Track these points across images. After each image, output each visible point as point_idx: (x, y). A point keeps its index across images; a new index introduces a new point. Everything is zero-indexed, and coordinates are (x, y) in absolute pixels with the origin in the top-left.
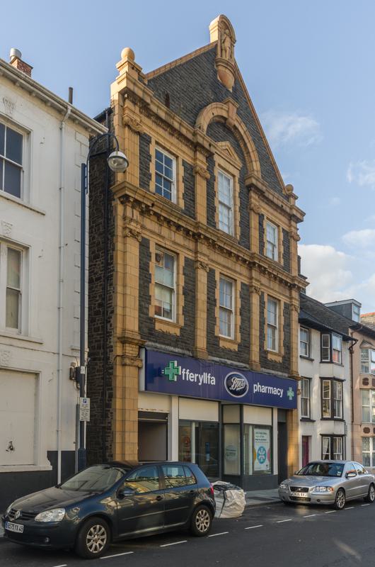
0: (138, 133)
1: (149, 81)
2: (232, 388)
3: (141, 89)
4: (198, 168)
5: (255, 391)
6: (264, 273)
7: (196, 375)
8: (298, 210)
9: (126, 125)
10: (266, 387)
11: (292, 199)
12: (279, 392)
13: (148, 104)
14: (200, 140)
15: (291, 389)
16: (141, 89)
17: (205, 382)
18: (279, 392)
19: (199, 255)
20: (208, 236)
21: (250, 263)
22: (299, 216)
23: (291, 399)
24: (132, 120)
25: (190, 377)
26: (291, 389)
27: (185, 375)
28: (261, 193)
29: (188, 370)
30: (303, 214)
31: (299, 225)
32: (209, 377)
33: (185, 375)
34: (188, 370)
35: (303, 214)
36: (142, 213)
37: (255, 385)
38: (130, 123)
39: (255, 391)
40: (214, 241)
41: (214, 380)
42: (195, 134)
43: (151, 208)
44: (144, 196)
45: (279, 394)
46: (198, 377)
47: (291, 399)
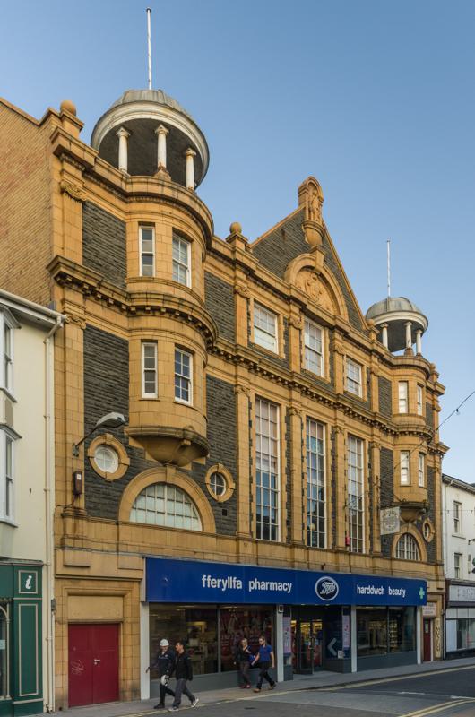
0: (79, 200)
1: (254, 250)
2: (322, 592)
3: (105, 168)
4: (292, 320)
5: (251, 588)
6: (307, 394)
7: (219, 580)
8: (440, 385)
9: (63, 191)
10: (267, 583)
11: (435, 377)
12: (286, 587)
13: (92, 167)
14: (238, 256)
15: (422, 589)
16: (105, 168)
17: (230, 586)
18: (286, 587)
19: (239, 379)
20: (302, 384)
21: (289, 383)
22: (440, 390)
23: (422, 597)
24: (70, 186)
25: (212, 583)
26: (422, 589)
27: (206, 582)
28: (346, 335)
29: (209, 577)
30: (443, 388)
31: (440, 398)
32: (234, 581)
33: (206, 582)
34: (209, 577)
35: (443, 388)
36: (86, 296)
37: (250, 583)
38: (68, 189)
39: (251, 588)
40: (255, 364)
41: (241, 584)
42: (233, 252)
43: (97, 289)
44: (147, 298)
45: (285, 590)
46: (221, 583)
47: (422, 597)
